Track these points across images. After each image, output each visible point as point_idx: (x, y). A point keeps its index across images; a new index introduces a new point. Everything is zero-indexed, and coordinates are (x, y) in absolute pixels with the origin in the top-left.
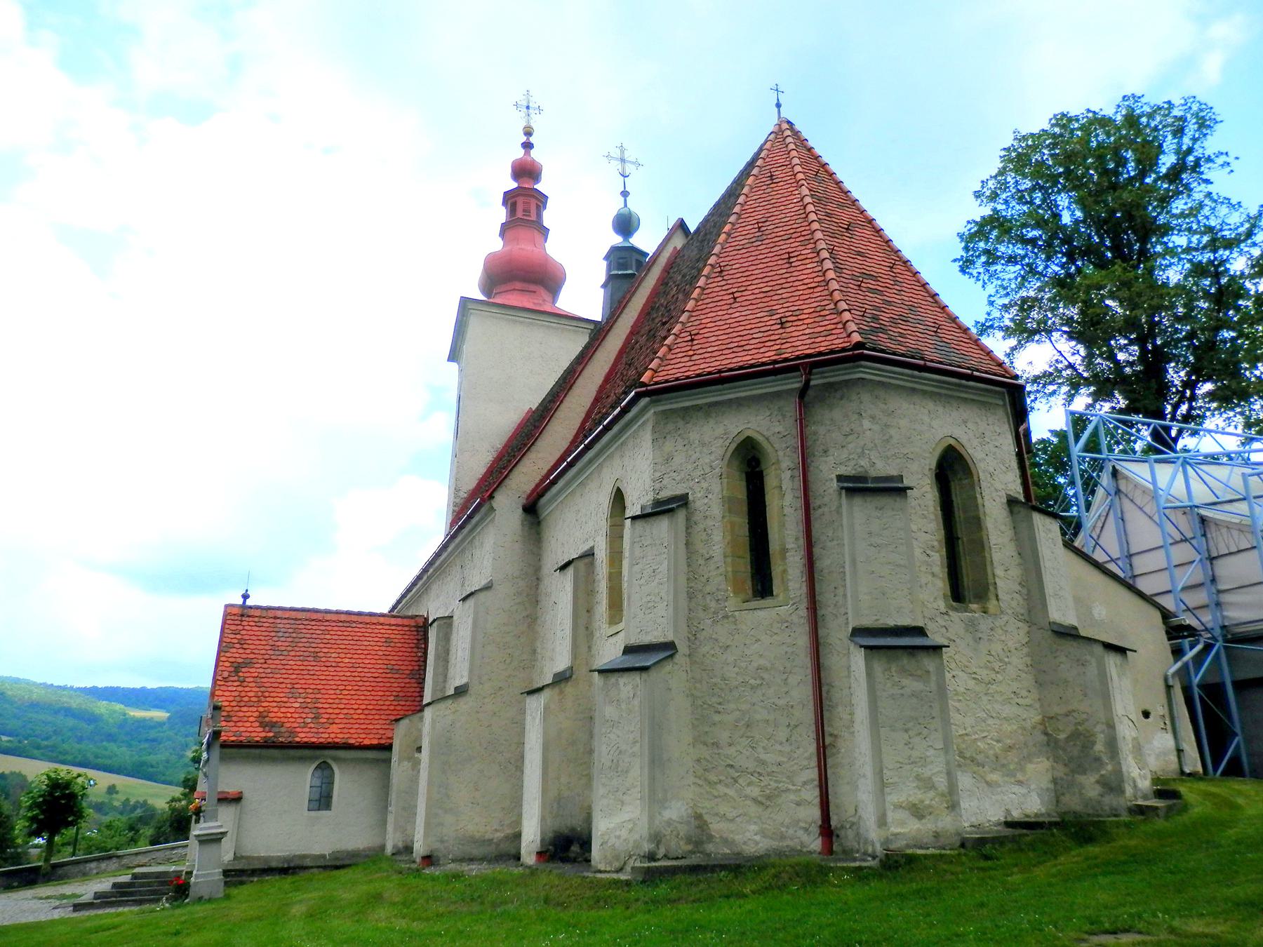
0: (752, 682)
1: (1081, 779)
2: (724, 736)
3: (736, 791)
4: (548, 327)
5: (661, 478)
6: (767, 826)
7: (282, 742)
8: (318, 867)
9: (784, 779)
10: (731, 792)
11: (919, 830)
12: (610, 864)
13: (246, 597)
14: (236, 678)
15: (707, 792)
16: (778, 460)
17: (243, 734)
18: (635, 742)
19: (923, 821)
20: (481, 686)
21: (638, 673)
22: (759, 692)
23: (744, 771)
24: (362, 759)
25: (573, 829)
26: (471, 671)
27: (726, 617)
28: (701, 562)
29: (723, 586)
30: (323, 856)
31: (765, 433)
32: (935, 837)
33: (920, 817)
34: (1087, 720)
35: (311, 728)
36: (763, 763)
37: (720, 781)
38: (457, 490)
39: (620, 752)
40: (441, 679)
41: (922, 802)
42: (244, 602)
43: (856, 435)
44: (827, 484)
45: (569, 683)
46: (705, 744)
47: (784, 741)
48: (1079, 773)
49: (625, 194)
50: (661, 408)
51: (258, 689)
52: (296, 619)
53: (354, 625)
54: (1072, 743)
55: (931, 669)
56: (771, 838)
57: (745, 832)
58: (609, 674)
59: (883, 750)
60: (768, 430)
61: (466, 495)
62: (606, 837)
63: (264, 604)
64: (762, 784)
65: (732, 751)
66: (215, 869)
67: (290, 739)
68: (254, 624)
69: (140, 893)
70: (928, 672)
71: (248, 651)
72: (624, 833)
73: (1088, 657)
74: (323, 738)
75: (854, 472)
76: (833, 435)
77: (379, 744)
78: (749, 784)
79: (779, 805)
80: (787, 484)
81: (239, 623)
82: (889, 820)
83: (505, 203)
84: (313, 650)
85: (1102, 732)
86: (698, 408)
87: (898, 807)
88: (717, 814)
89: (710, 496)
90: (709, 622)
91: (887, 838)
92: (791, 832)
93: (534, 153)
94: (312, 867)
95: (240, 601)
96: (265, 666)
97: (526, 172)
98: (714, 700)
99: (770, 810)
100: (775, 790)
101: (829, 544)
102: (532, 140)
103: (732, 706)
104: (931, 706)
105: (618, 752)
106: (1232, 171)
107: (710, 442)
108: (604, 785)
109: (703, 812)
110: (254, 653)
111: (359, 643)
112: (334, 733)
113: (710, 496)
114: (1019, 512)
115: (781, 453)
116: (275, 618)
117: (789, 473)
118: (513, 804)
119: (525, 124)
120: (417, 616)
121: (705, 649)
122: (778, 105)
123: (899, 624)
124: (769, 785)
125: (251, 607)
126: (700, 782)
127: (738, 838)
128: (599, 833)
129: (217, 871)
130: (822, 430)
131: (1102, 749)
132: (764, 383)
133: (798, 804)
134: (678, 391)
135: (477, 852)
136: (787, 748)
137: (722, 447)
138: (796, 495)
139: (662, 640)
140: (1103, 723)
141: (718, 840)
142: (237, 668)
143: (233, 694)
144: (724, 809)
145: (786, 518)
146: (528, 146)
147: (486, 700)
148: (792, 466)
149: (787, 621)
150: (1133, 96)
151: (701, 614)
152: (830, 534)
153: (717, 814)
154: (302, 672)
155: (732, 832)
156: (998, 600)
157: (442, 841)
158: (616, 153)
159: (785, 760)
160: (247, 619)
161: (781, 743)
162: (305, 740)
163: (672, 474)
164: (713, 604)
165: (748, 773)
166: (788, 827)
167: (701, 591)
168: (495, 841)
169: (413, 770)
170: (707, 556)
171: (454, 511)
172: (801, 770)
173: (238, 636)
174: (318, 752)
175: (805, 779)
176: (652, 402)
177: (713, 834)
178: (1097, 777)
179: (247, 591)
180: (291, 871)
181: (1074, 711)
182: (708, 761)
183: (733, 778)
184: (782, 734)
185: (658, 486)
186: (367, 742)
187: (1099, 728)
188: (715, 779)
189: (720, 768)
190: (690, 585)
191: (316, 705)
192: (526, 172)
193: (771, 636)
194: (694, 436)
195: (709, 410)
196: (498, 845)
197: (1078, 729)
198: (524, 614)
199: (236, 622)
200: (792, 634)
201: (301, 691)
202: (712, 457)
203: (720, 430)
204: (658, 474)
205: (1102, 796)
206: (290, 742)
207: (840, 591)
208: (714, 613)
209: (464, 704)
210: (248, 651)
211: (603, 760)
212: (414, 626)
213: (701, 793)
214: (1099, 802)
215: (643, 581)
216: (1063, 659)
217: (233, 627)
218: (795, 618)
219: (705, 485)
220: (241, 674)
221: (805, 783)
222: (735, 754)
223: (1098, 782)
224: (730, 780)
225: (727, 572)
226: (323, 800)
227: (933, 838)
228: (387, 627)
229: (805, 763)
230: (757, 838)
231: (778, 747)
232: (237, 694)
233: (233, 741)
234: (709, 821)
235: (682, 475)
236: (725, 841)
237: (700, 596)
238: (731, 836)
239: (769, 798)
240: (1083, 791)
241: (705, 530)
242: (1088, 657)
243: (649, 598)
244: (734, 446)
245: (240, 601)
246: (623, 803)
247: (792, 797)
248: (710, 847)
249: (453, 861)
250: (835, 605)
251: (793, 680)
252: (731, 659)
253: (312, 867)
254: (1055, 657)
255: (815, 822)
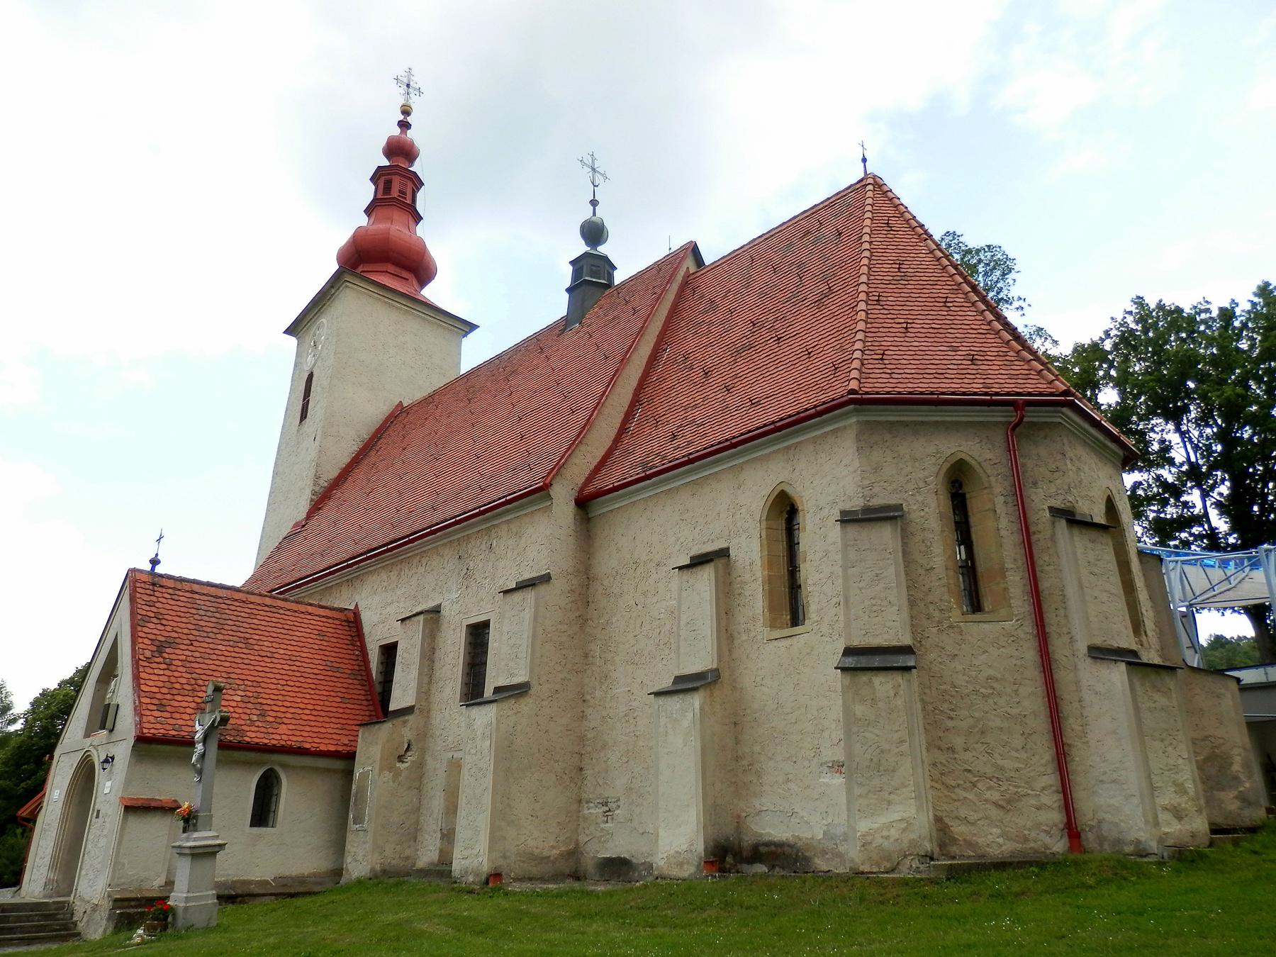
0: (983, 690)
1: (1222, 795)
2: (959, 742)
3: (976, 795)
4: (424, 319)
5: (871, 486)
6: (1010, 829)
7: (230, 741)
8: (272, 894)
9: (1023, 785)
10: (971, 796)
11: (1180, 830)
12: (878, 865)
13: (155, 562)
14: (160, 660)
15: (946, 796)
16: (990, 485)
17: (183, 728)
18: (902, 741)
19: (1182, 823)
20: (540, 687)
21: (900, 672)
22: (991, 701)
23: (983, 776)
24: (313, 767)
25: (727, 839)
26: (531, 671)
27: (951, 627)
28: (922, 571)
29: (946, 597)
30: (266, 882)
31: (977, 458)
32: (1192, 836)
33: (1180, 818)
34: (1224, 744)
35: (258, 727)
36: (1002, 769)
37: (959, 785)
38: (317, 477)
39: (882, 751)
40: (426, 680)
41: (1180, 805)
42: (153, 568)
43: (1062, 473)
44: (1040, 513)
45: (717, 686)
46: (940, 748)
47: (1020, 747)
48: (1218, 790)
49: (594, 203)
50: (865, 418)
51: (189, 676)
52: (216, 597)
53: (282, 611)
54: (1209, 764)
55: (1172, 688)
56: (1014, 841)
57: (988, 835)
58: (859, 673)
59: (1150, 758)
60: (979, 456)
61: (326, 484)
62: (869, 838)
63: (176, 573)
64: (1002, 789)
65: (968, 756)
66: (207, 890)
67: (239, 739)
68: (169, 596)
69: (22, 930)
70: (1170, 689)
71: (169, 628)
72: (894, 833)
73: (1223, 691)
74: (275, 740)
75: (1063, 506)
76: (1040, 469)
77: (336, 751)
78: (989, 789)
79: (1020, 809)
80: (1001, 509)
81: (152, 593)
82: (1160, 821)
83: (375, 179)
84: (242, 635)
85: (1240, 755)
86: (905, 424)
87: (1165, 809)
88: (957, 818)
89: (926, 509)
90: (934, 630)
91: (1161, 837)
92: (1033, 834)
93: (410, 134)
94: (264, 895)
95: (148, 567)
96: (191, 648)
97: (400, 151)
98: (946, 706)
99: (1011, 814)
100: (1015, 794)
101: (1047, 568)
102: (409, 119)
103: (964, 713)
104: (1175, 720)
105: (878, 751)
106: (1024, 315)
107: (922, 459)
108: (861, 784)
109: (944, 814)
110: (176, 632)
111: (290, 632)
112: (281, 735)
113: (926, 509)
114: (1148, 561)
115: (993, 479)
116: (193, 592)
117: (1002, 499)
118: (568, 819)
119: (402, 102)
120: (346, 609)
121: (932, 656)
122: (864, 160)
123: (1121, 646)
124: (1009, 789)
125: (161, 576)
126: (938, 786)
127: (981, 840)
128: (859, 834)
129: (210, 893)
130: (1030, 464)
131: (1240, 769)
132: (956, 411)
133: (1038, 809)
134: (890, 405)
135: (535, 871)
136: (1024, 755)
137: (935, 464)
138: (1011, 520)
139: (895, 643)
140: (1239, 747)
141: (961, 843)
142: (160, 648)
143: (162, 678)
144: (963, 812)
145: (1004, 540)
146: (404, 125)
147: (544, 703)
148: (1004, 492)
149: (1013, 636)
150: (954, 233)
151: (925, 623)
152: (1047, 559)
153: (957, 818)
154: (236, 660)
155: (975, 835)
156: (1146, 636)
157: (505, 857)
158: (588, 160)
159: (1022, 766)
160: (160, 589)
161: (1017, 751)
162: (256, 740)
163: (882, 483)
164: (937, 614)
165: (987, 778)
166: (1029, 830)
167: (922, 600)
168: (552, 858)
169: (394, 782)
170: (928, 567)
171: (312, 500)
172: (1039, 776)
173: (154, 609)
174: (266, 757)
175: (1043, 785)
176: (856, 410)
177: (956, 836)
178: (1236, 793)
179: (157, 555)
180: (239, 899)
181: (1211, 736)
182: (945, 766)
183: (972, 783)
184: (1017, 742)
185: (867, 492)
186: (323, 748)
187: (1235, 751)
188: (953, 783)
189: (957, 773)
190: (911, 593)
191: (259, 700)
192: (400, 151)
193: (998, 649)
194: (904, 449)
195: (917, 428)
196: (554, 863)
197: (1214, 752)
198: (577, 614)
199: (148, 592)
200: (1020, 648)
201: (239, 682)
202: (926, 473)
203: (931, 449)
204: (867, 482)
205: (1241, 809)
206: (239, 742)
207: (1062, 612)
208: (939, 622)
209: (526, 705)
210: (169, 628)
211: (857, 760)
212: (345, 621)
213: (939, 797)
214: (1239, 815)
215: (862, 584)
216: (1198, 691)
217: (146, 598)
218: (1020, 633)
219: (920, 498)
220: (164, 655)
221: (1043, 789)
222: (971, 760)
223: (1236, 797)
224: (968, 784)
225: (949, 584)
226: (262, 814)
227: (1190, 838)
228: (317, 618)
229: (1042, 769)
230: (1000, 840)
231: (1014, 754)
232: (165, 679)
233: (174, 736)
234: (950, 824)
235: (894, 486)
236: (969, 844)
237: (921, 605)
238: (974, 838)
239: (1009, 802)
240: (1223, 805)
241: (923, 542)
242: (1223, 691)
243: (873, 602)
244: (947, 465)
245: (148, 567)
246: (889, 803)
247: (1033, 802)
248: (954, 850)
249: (515, 880)
250: (1058, 624)
251: (1024, 691)
252: (960, 667)
253: (264, 895)
254: (1190, 690)
255: (1056, 826)
